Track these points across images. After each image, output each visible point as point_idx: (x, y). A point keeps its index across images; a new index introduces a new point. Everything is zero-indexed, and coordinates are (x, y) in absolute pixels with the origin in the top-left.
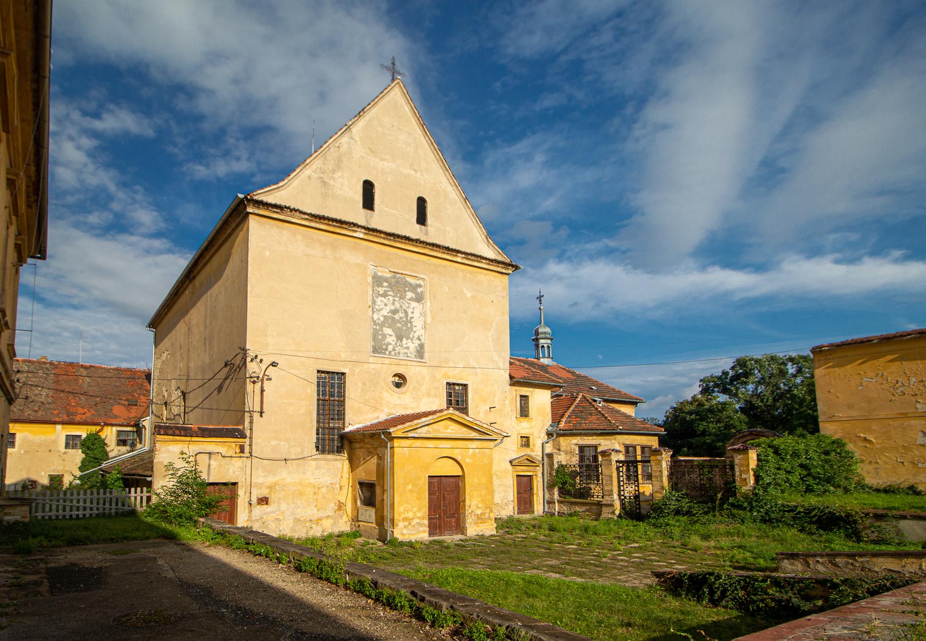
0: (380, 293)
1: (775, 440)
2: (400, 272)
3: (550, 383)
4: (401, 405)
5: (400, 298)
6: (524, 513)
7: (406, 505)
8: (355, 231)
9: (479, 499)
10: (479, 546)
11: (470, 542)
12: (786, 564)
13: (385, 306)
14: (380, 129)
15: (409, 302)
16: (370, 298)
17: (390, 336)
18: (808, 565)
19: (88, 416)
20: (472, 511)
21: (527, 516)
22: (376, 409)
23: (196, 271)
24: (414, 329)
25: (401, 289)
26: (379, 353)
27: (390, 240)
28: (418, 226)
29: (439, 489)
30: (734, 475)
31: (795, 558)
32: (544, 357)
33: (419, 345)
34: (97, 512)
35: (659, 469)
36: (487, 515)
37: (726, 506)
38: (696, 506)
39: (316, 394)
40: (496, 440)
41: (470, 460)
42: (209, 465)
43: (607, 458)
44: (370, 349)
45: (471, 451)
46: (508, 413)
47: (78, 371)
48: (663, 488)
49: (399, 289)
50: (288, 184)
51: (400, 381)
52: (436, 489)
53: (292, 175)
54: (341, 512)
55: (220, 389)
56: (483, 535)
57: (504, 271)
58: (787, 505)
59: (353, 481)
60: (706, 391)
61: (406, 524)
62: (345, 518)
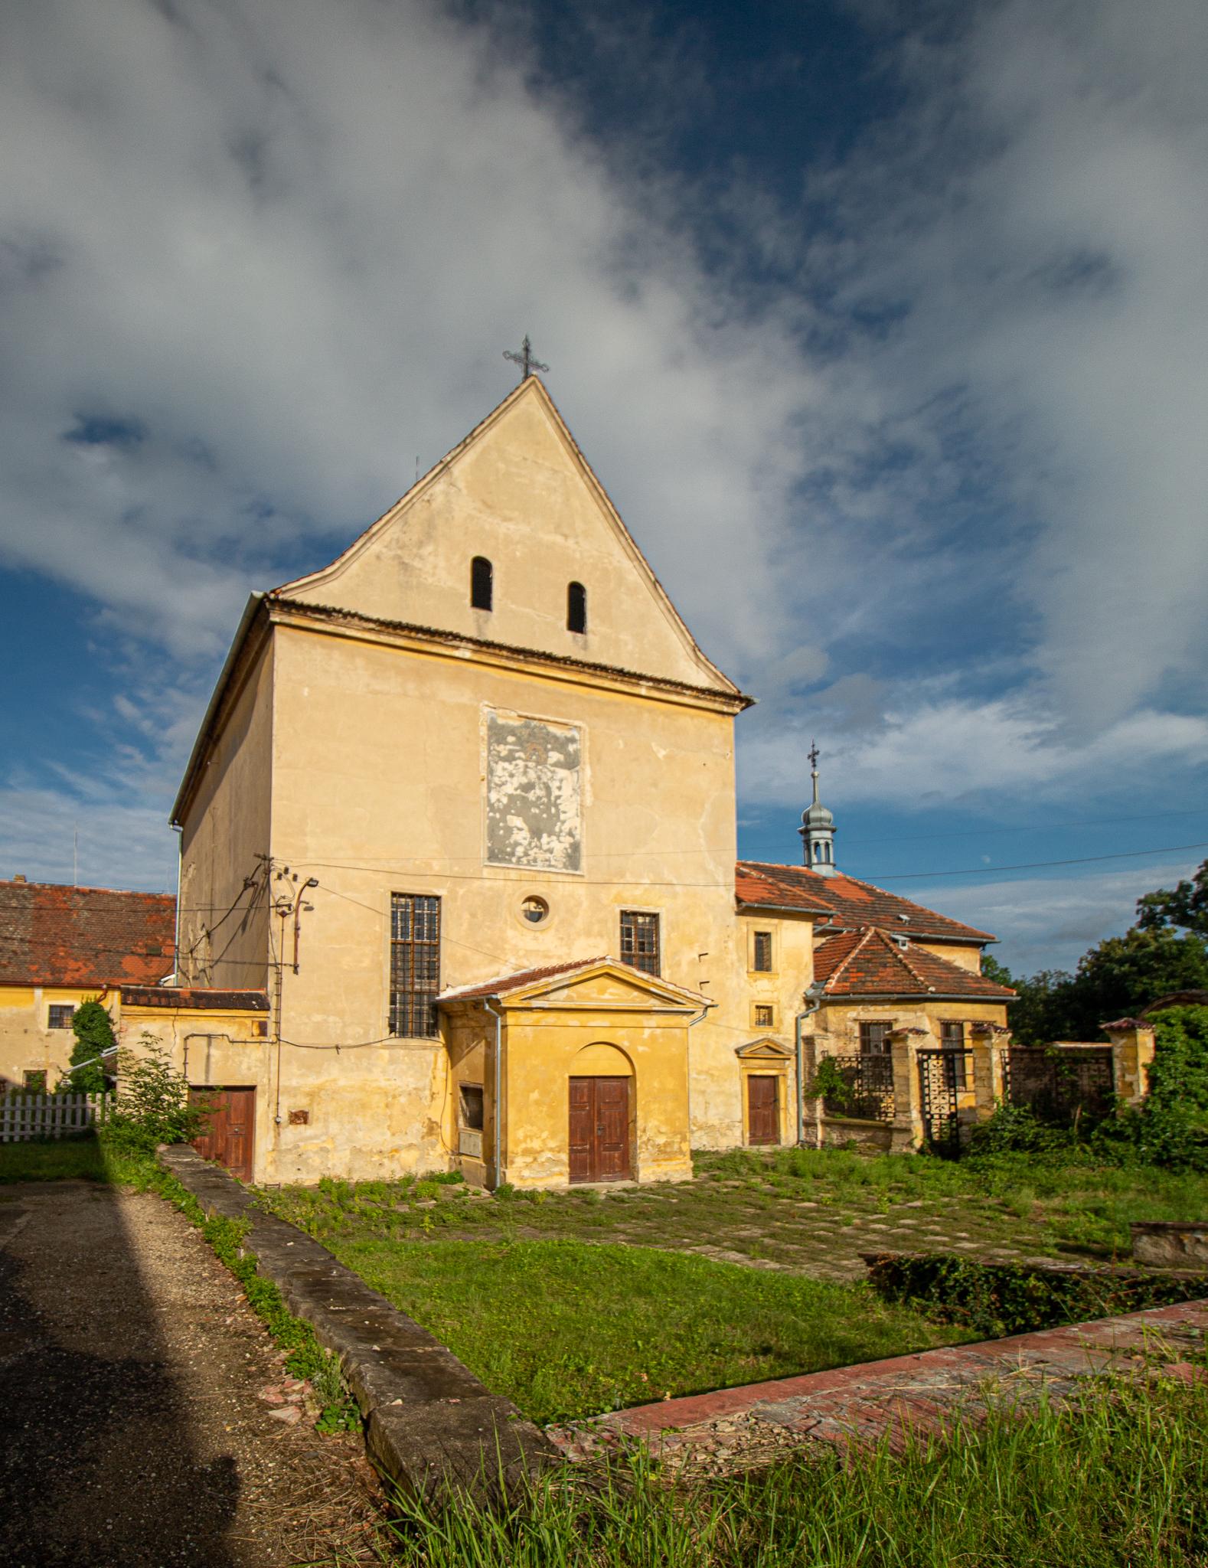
0: (502, 754)
1: (1195, 1010)
2: (537, 716)
3: (809, 910)
4: (538, 951)
5: (538, 763)
6: (764, 1142)
7: (529, 1127)
8: (457, 648)
9: (662, 1118)
10: (650, 1200)
11: (640, 1194)
12: (1147, 1246)
13: (511, 778)
14: (502, 466)
15: (552, 769)
16: (483, 765)
17: (520, 829)
18: (1181, 1245)
19: (85, 973)
20: (649, 1140)
21: (766, 1149)
22: (494, 959)
23: (219, 726)
24: (562, 817)
25: (538, 747)
26: (500, 860)
27: (519, 660)
28: (570, 634)
29: (591, 1101)
30: (1111, 1076)
31: (1160, 1233)
32: (819, 863)
33: (572, 845)
34: (31, 1133)
35: (987, 1065)
36: (676, 1147)
37: (1095, 1134)
38: (1048, 1132)
39: (389, 934)
40: (693, 1013)
41: (646, 1049)
42: (208, 1057)
43: (901, 1045)
44: (484, 854)
45: (647, 1032)
46: (732, 964)
47: (71, 899)
48: (992, 1099)
49: (535, 746)
50: (343, 569)
51: (538, 909)
52: (585, 1099)
53: (348, 554)
54: (433, 1138)
55: (244, 925)
56: (668, 1182)
57: (725, 709)
58: (1202, 1133)
59: (454, 1085)
60: (1150, 920)
61: (529, 1159)
62: (440, 1149)
